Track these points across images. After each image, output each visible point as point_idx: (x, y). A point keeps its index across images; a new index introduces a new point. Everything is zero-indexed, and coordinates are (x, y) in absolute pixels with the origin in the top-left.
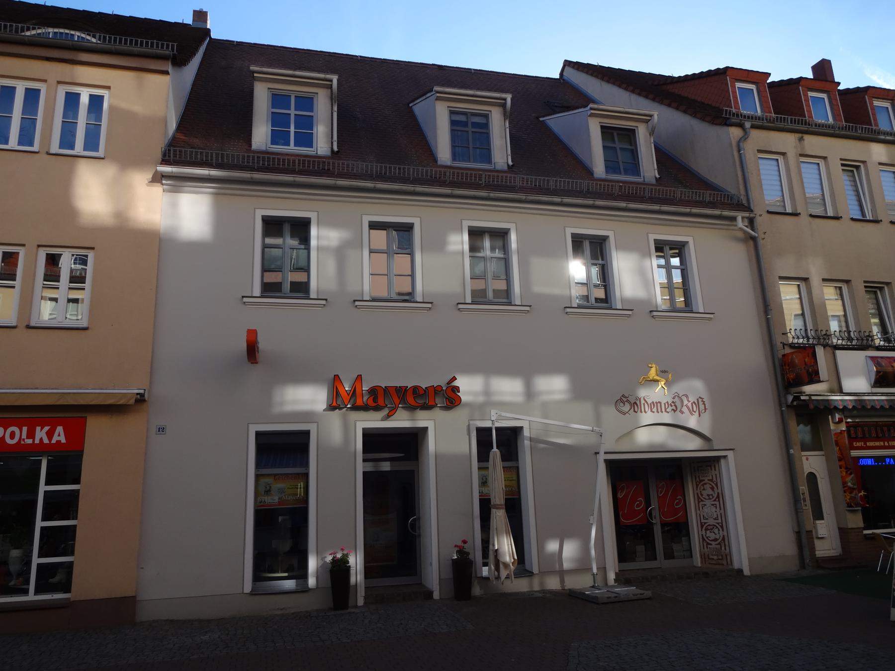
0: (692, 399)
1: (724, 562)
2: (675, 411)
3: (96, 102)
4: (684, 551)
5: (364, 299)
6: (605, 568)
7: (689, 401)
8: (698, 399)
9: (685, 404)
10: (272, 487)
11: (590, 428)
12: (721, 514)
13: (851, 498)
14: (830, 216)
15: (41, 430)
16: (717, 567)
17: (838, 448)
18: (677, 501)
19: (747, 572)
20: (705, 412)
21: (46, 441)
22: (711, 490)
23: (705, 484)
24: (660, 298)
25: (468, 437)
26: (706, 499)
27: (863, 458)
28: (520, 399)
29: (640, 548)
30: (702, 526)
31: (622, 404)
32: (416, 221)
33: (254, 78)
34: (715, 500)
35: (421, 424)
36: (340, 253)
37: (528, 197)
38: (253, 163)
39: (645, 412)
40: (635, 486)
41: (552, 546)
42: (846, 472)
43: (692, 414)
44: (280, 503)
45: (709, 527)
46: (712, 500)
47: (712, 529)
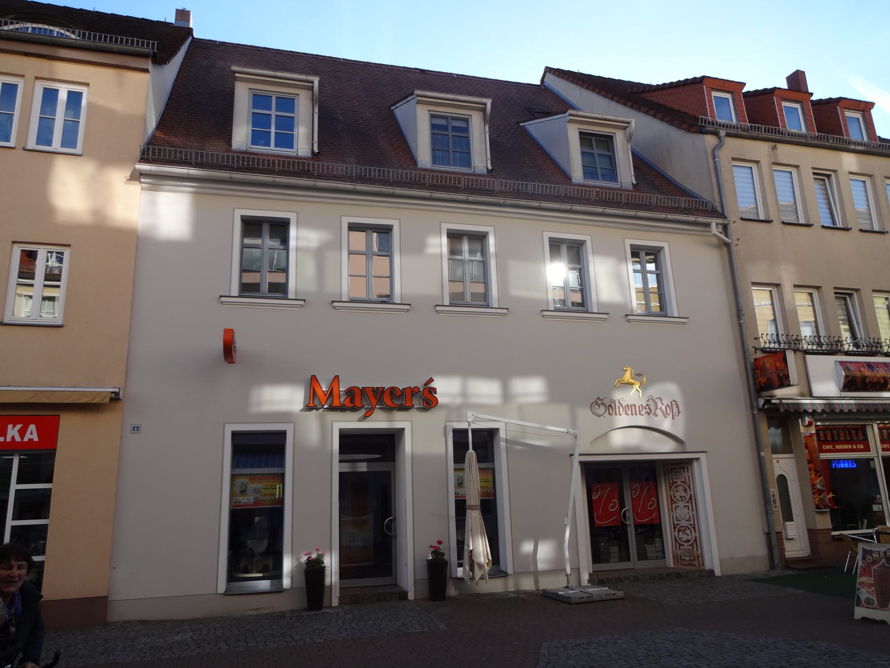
0: (666, 402)
2: (649, 414)
4: (657, 552)
5: (343, 300)
6: (579, 568)
8: (671, 402)
9: (658, 407)
10: (248, 488)
11: (565, 430)
12: (693, 515)
13: (820, 500)
15: (13, 428)
19: (718, 573)
20: (679, 414)
21: (18, 439)
22: (683, 492)
23: (679, 486)
24: (636, 303)
25: (444, 438)
28: (497, 401)
29: (614, 550)
30: (675, 528)
31: (597, 407)
32: (395, 224)
33: (235, 79)
34: (687, 502)
35: (398, 425)
36: (319, 254)
39: (620, 415)
42: (815, 475)
43: (666, 417)
44: (255, 504)
45: (681, 529)
46: (684, 502)
47: (684, 531)
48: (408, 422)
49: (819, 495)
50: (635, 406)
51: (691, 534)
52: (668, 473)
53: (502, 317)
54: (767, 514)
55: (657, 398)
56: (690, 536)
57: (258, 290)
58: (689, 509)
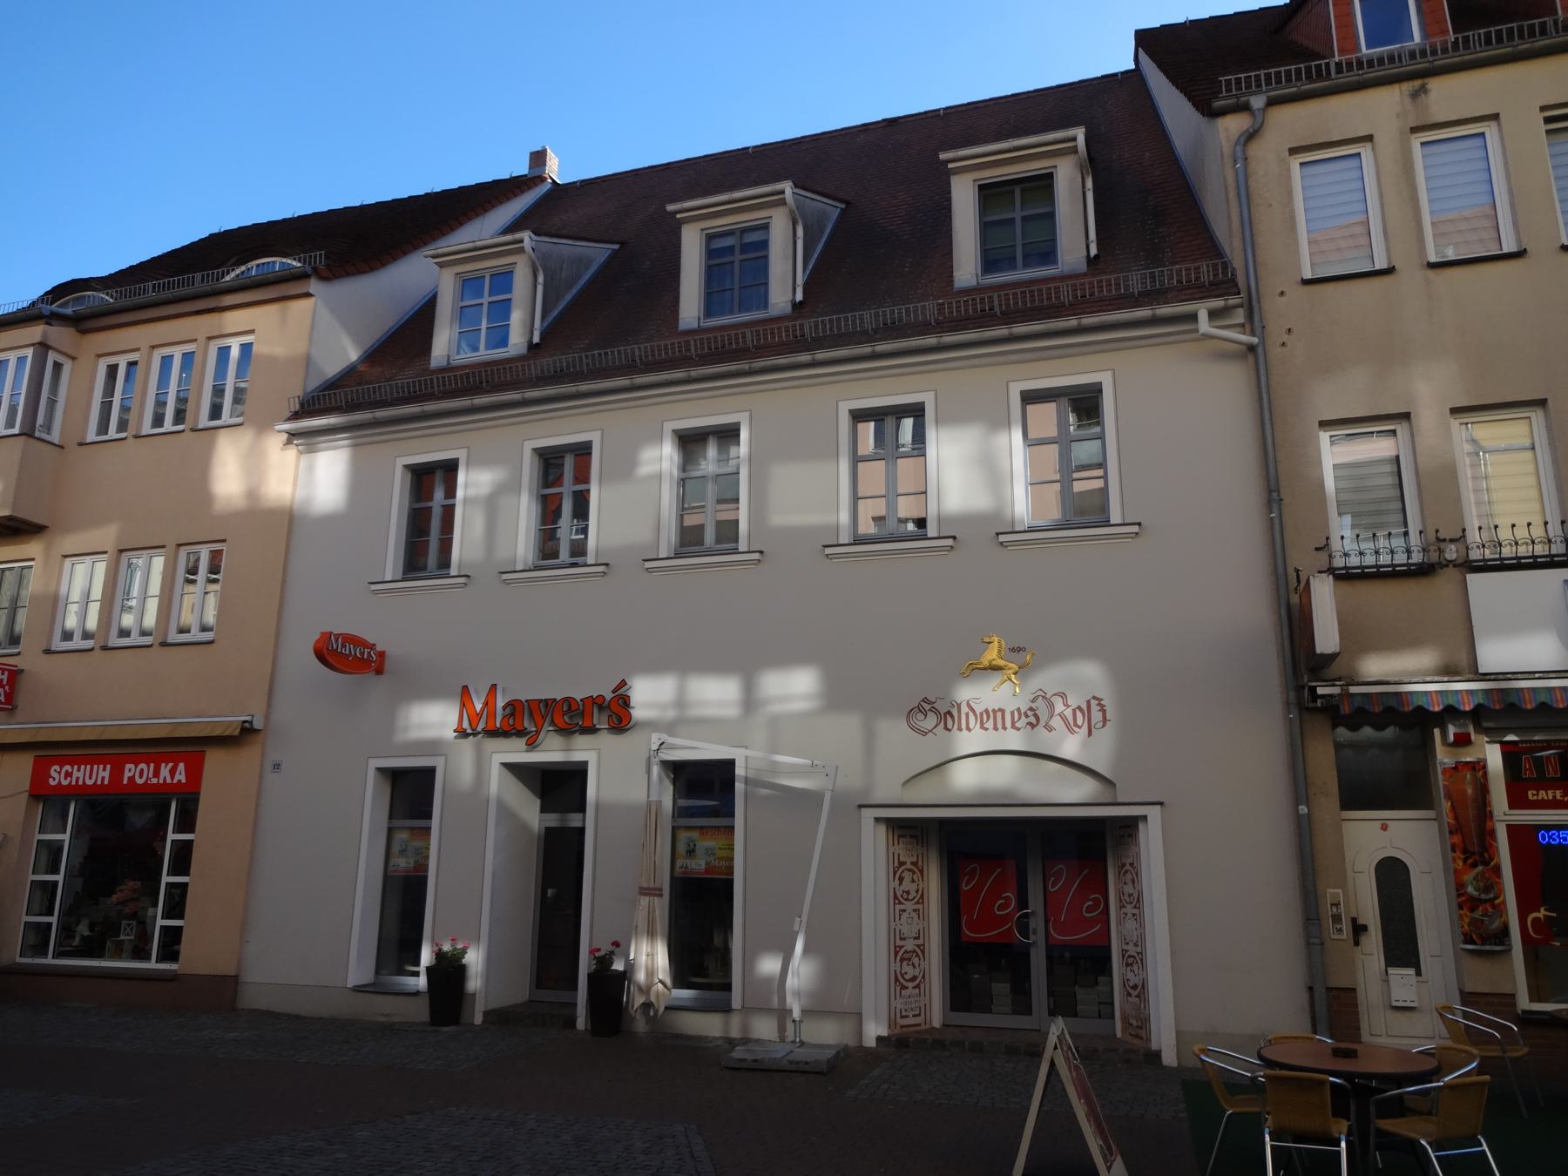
0: (1073, 701)
2: (1033, 726)
3: (246, 349)
4: (1099, 1003)
5: (1017, 529)
6: (861, 1014)
7: (1068, 706)
8: (1088, 703)
9: (1057, 712)
10: (697, 847)
13: (1473, 922)
14: (1381, 270)
15: (166, 766)
17: (1449, 804)
18: (1003, 901)
19: (1169, 1058)
20: (1103, 726)
21: (169, 781)
24: (1021, 505)
25: (647, 776)
27: (1548, 828)
28: (733, 712)
29: (1001, 989)
30: (896, 953)
31: (921, 716)
32: (1106, 379)
33: (680, 223)
35: (577, 756)
36: (491, 504)
37: (753, 365)
38: (386, 396)
39: (969, 729)
41: (769, 965)
42: (1465, 861)
43: (1071, 731)
44: (707, 871)
48: (593, 752)
49: (1472, 910)
50: (1002, 711)
53: (1130, 540)
55: (1055, 694)
57: (701, 542)
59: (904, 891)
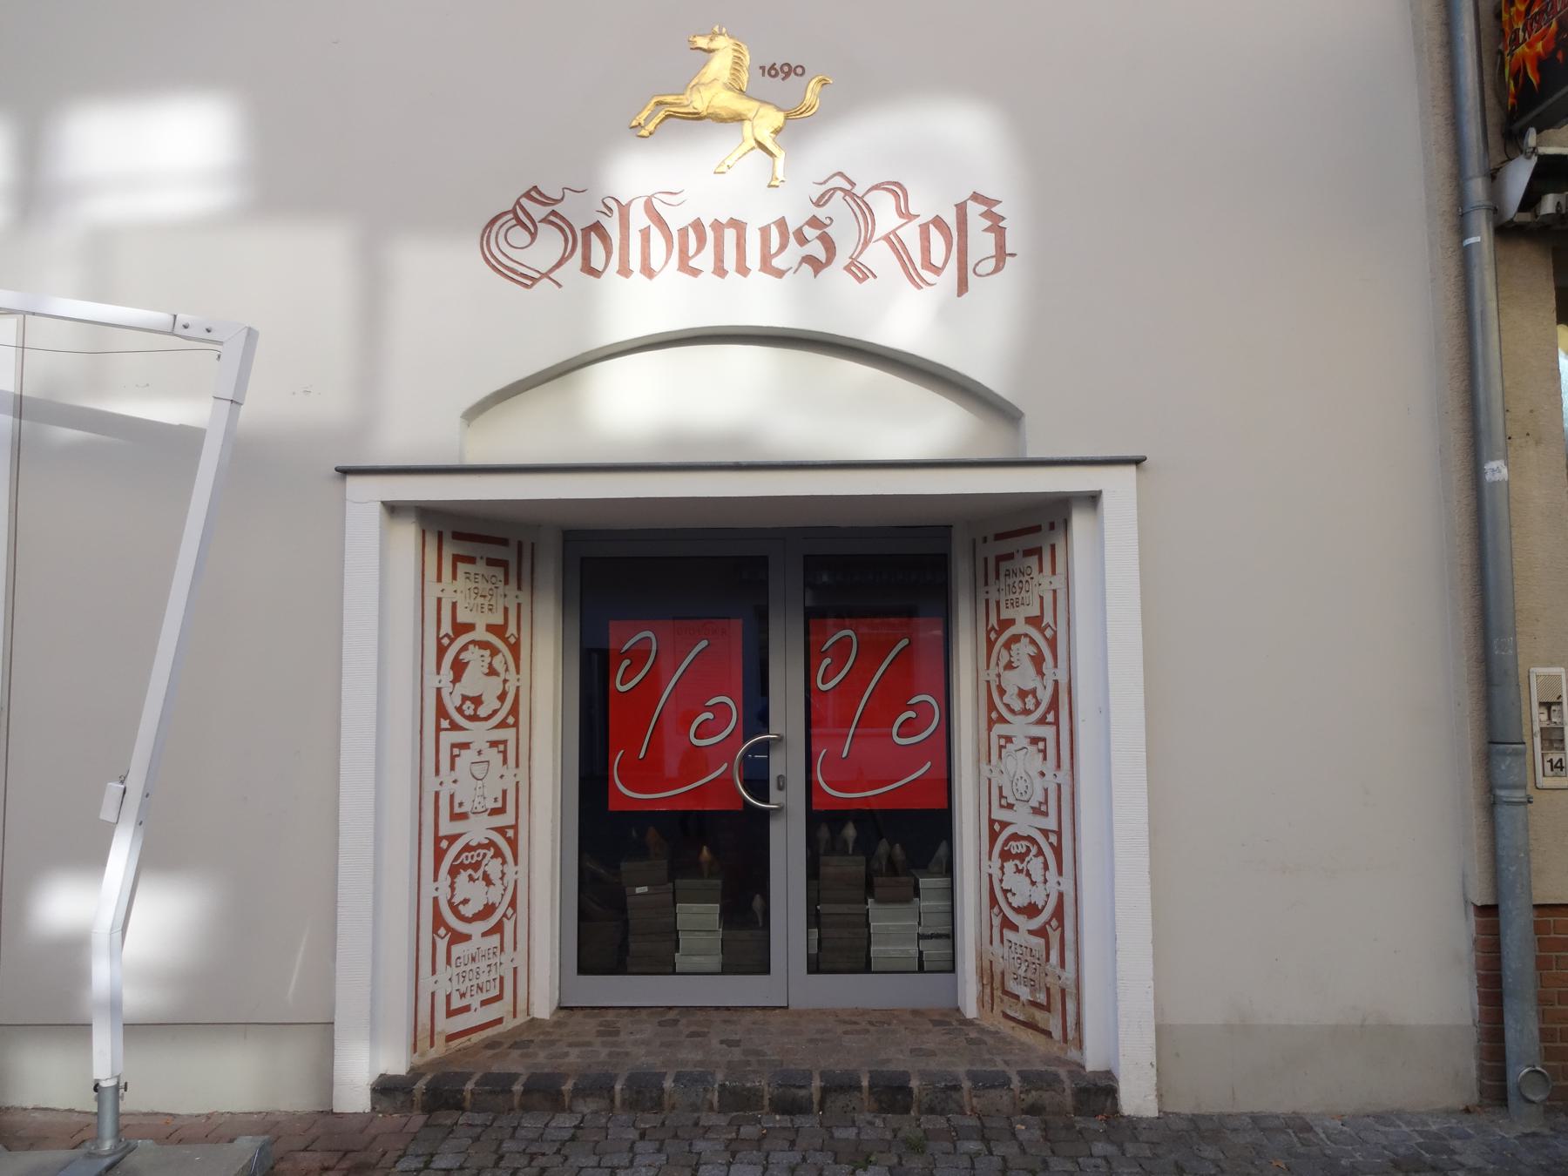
0: (924, 205)
1: (1054, 1025)
2: (816, 265)
4: (921, 937)
8: (961, 209)
9: (878, 233)
11: (160, 317)
16: (1026, 1036)
18: (911, 714)
20: (997, 269)
22: (1031, 670)
23: (1016, 639)
26: (1012, 711)
31: (519, 236)
39: (648, 271)
40: (704, 643)
43: (917, 282)
47: (1021, 857)
50: (739, 226)
51: (1045, 881)
52: (986, 584)
54: (1491, 804)
55: (876, 187)
56: (1040, 886)
58: (1044, 751)
59: (465, 698)
